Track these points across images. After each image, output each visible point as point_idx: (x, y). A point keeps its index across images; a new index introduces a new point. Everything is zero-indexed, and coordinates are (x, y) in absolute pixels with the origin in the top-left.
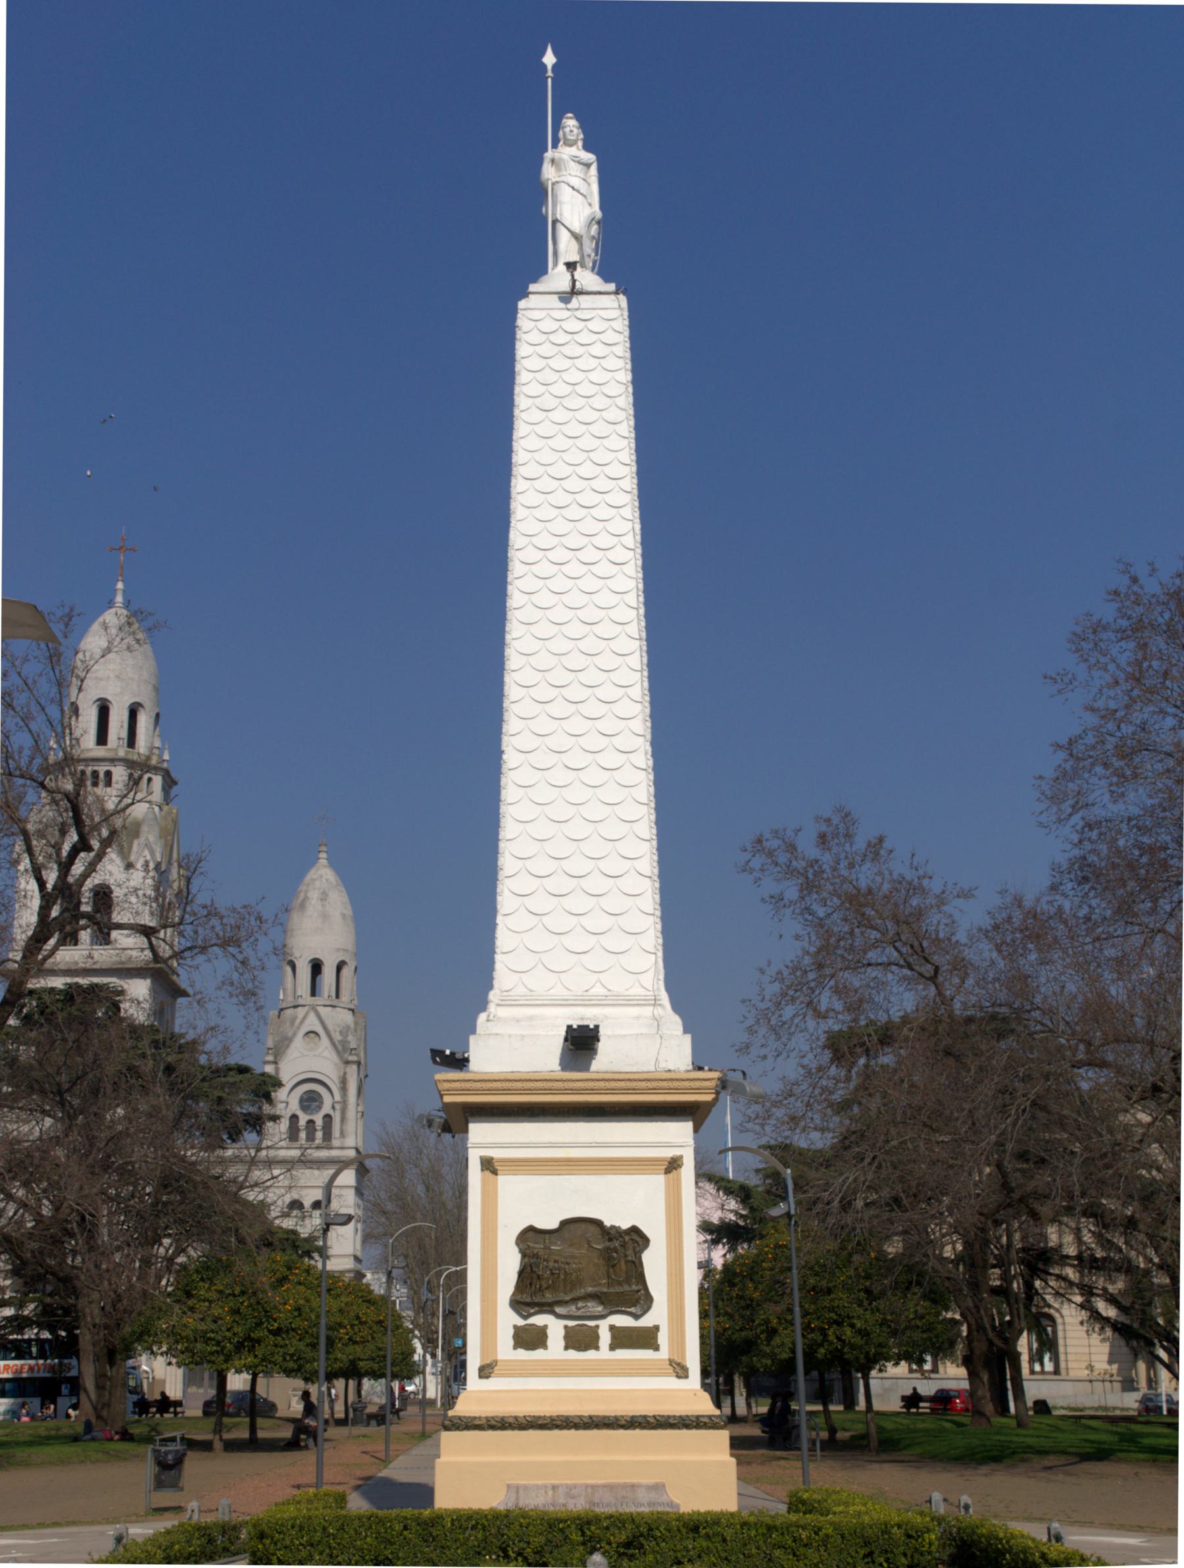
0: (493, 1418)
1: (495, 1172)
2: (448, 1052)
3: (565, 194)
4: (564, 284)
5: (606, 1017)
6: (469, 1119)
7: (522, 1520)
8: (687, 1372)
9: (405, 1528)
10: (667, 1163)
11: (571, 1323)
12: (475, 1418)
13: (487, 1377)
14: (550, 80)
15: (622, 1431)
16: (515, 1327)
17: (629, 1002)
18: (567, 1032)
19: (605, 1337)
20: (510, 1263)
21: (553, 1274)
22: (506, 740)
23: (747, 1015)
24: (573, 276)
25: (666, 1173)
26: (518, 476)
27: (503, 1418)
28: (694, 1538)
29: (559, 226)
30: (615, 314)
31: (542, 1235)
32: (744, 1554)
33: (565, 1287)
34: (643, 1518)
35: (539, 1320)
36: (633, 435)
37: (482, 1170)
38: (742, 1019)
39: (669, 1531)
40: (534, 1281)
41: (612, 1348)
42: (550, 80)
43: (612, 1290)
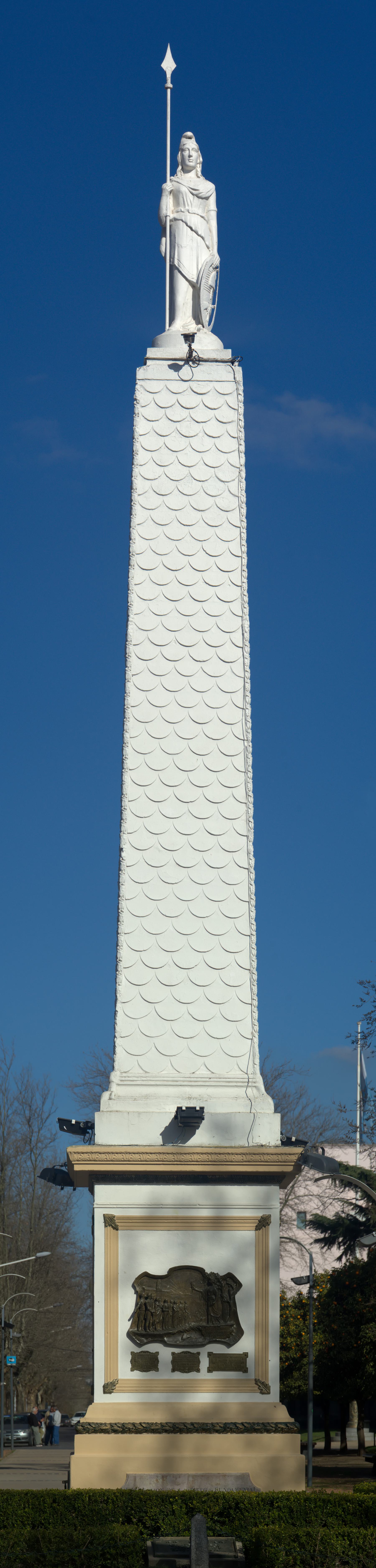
0: (116, 1424)
1: (116, 1228)
2: (73, 1122)
3: (185, 237)
4: (181, 350)
5: (210, 1097)
6: (94, 1183)
7: (142, 1496)
8: (270, 1390)
9: (54, 1501)
10: (257, 1221)
11: (177, 1351)
12: (101, 1424)
13: (110, 1393)
14: (169, 91)
15: (217, 1435)
16: (132, 1353)
17: (229, 1083)
18: (177, 1112)
19: (205, 1363)
20: (127, 1303)
21: (163, 1311)
22: (125, 837)
23: (365, 997)
24: (190, 346)
25: (256, 1230)
26: (136, 566)
27: (123, 1425)
28: (270, 1509)
29: (176, 272)
30: (230, 387)
31: (155, 1280)
32: (306, 1521)
33: (173, 1322)
34: (231, 1495)
35: (153, 1347)
36: (245, 524)
37: (106, 1226)
38: (360, 1003)
39: (251, 1504)
40: (149, 1317)
41: (210, 1370)
42: (169, 91)
43: (211, 1324)
